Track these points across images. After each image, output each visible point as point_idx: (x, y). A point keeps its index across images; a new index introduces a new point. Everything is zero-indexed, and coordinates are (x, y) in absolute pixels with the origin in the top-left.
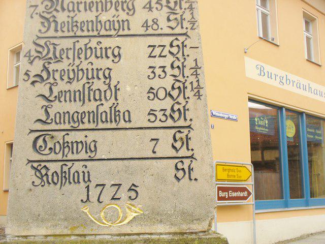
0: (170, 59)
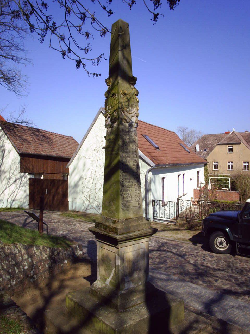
0: (138, 191)
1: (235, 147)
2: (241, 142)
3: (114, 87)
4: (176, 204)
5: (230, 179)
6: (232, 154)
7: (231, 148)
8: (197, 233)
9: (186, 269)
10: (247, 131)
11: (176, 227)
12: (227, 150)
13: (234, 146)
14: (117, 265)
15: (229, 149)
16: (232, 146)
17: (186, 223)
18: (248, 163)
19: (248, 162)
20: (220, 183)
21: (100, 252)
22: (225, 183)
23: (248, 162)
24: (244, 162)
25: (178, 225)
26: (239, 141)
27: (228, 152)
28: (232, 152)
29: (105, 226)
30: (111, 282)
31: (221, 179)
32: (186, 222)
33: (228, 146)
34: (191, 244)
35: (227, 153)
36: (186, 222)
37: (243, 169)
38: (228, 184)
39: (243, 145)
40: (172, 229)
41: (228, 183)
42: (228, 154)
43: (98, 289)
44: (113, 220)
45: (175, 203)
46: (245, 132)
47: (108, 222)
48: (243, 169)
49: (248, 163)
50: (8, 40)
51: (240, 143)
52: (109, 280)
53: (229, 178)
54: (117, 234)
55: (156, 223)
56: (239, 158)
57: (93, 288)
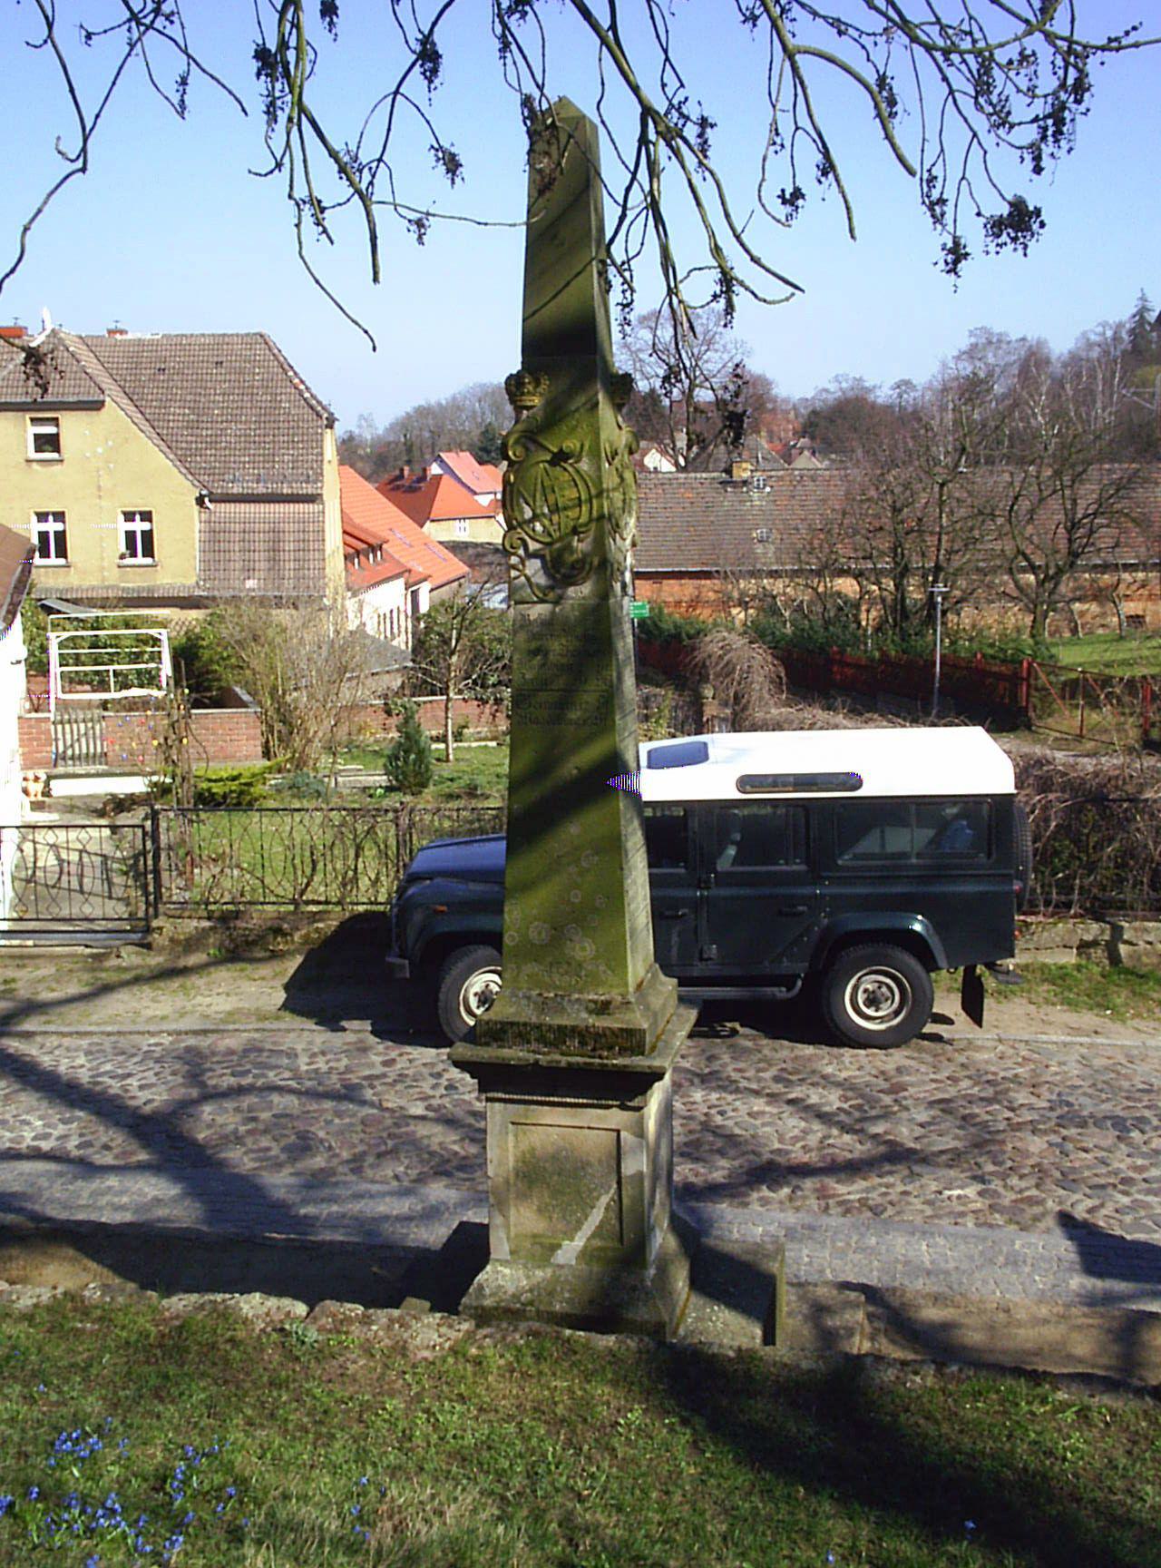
1: (72, 427)
2: (108, 399)
3: (561, 420)
4: (145, 834)
5: (164, 638)
6: (57, 468)
7: (51, 430)
8: (291, 971)
9: (435, 1148)
10: (120, 326)
11: (155, 960)
12: (26, 440)
13: (65, 418)
14: (632, 1176)
15: (37, 437)
16: (55, 421)
17: (211, 928)
18: (150, 521)
19: (150, 513)
20: (111, 662)
21: (511, 1145)
22: (136, 658)
23: (150, 513)
24: (125, 514)
25: (163, 948)
26: (94, 390)
27: (33, 455)
28: (55, 456)
29: (549, 1031)
30: (585, 1254)
31: (116, 637)
32: (206, 924)
33: (28, 416)
34: (315, 1027)
35: (29, 461)
36: (206, 924)
37: (122, 557)
38: (153, 665)
39: (115, 413)
40: (146, 972)
41: (156, 657)
42: (35, 466)
43: (515, 1297)
44: (595, 1002)
45: (139, 832)
46: (110, 332)
47: (562, 1011)
48: (122, 557)
49: (150, 521)
50: (710, 392)
51: (97, 406)
52: (571, 1250)
53: (163, 635)
54: (643, 1054)
55: (21, 957)
56: (99, 488)
57: (488, 1302)
